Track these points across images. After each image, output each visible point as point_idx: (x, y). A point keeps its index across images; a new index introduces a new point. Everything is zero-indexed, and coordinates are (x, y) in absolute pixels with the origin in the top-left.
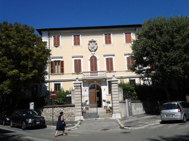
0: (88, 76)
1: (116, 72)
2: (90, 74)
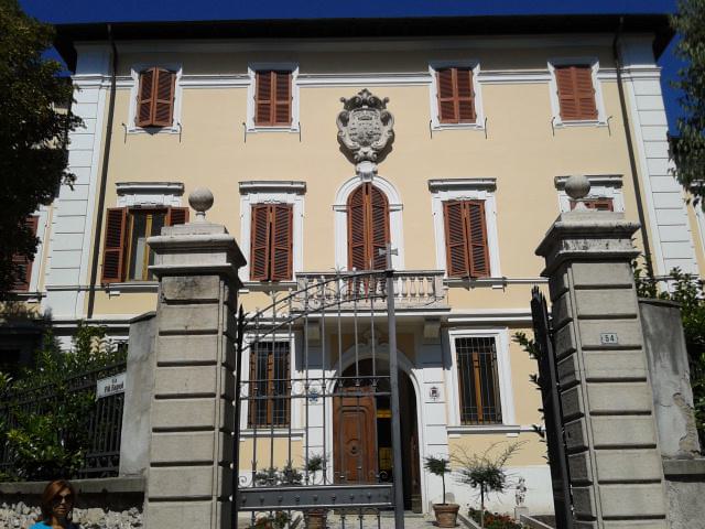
1: (504, 282)
2: (343, 287)
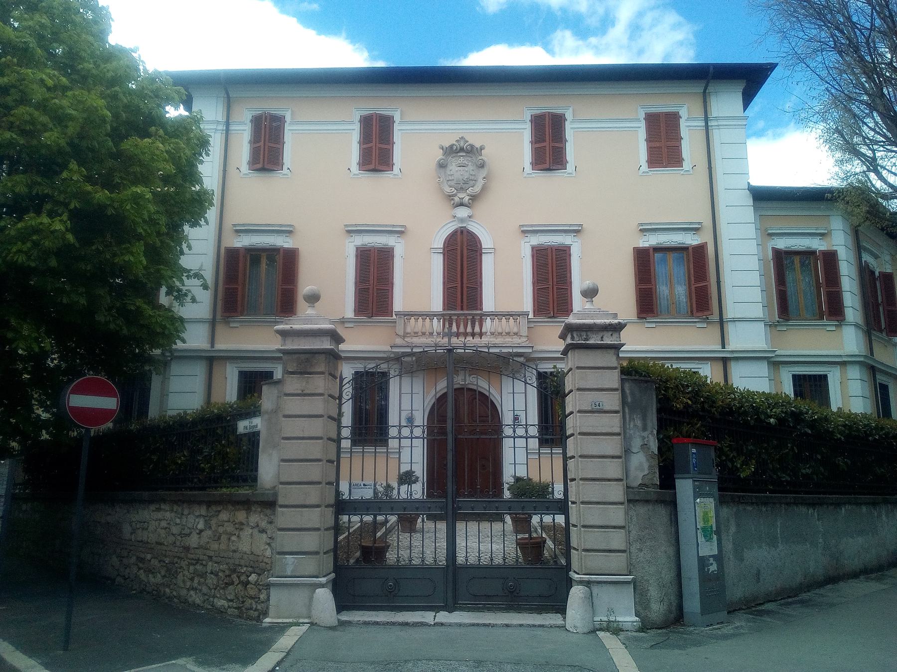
0: (430, 335)
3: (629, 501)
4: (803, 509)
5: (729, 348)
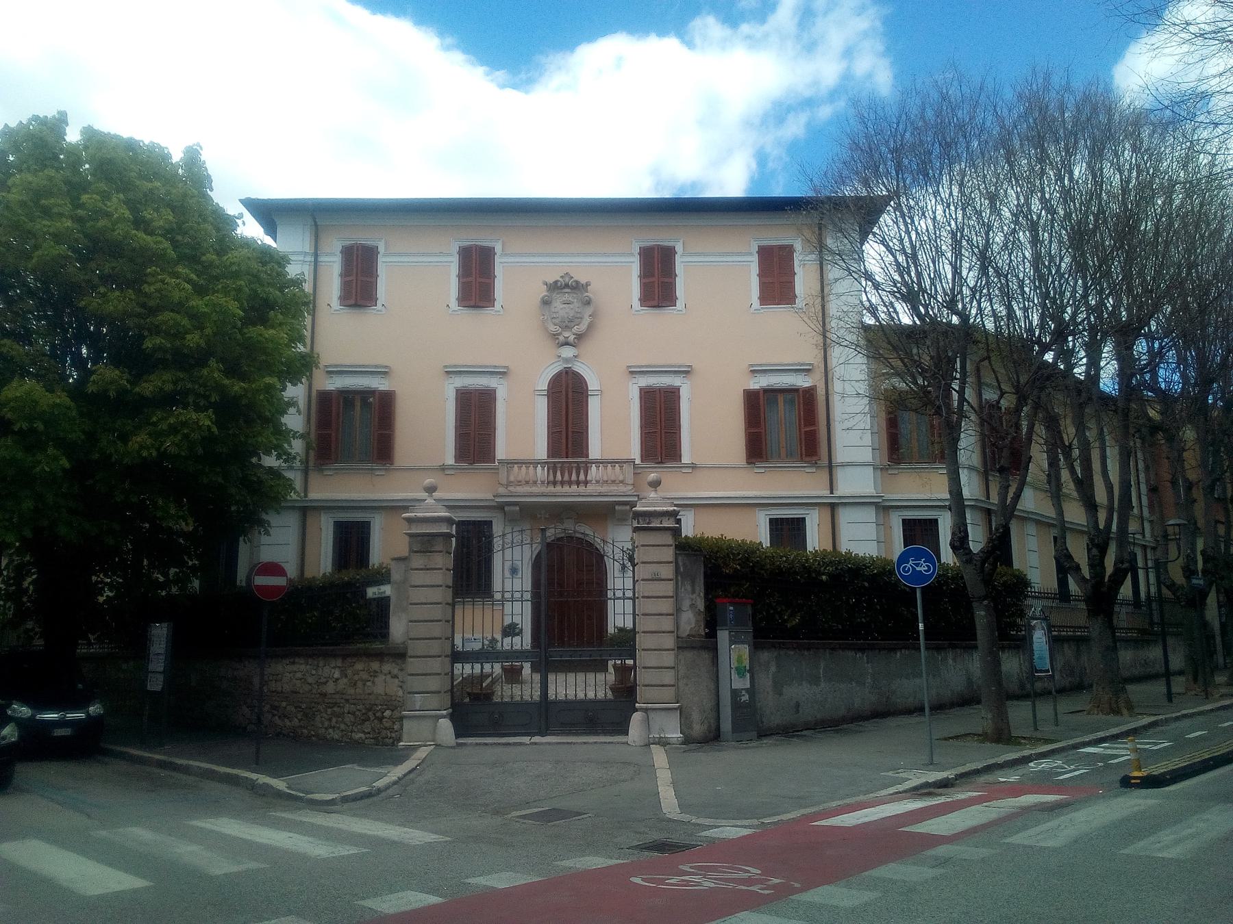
0: (537, 486)
1: (693, 467)
3: (679, 648)
4: (851, 654)
5: (838, 493)
